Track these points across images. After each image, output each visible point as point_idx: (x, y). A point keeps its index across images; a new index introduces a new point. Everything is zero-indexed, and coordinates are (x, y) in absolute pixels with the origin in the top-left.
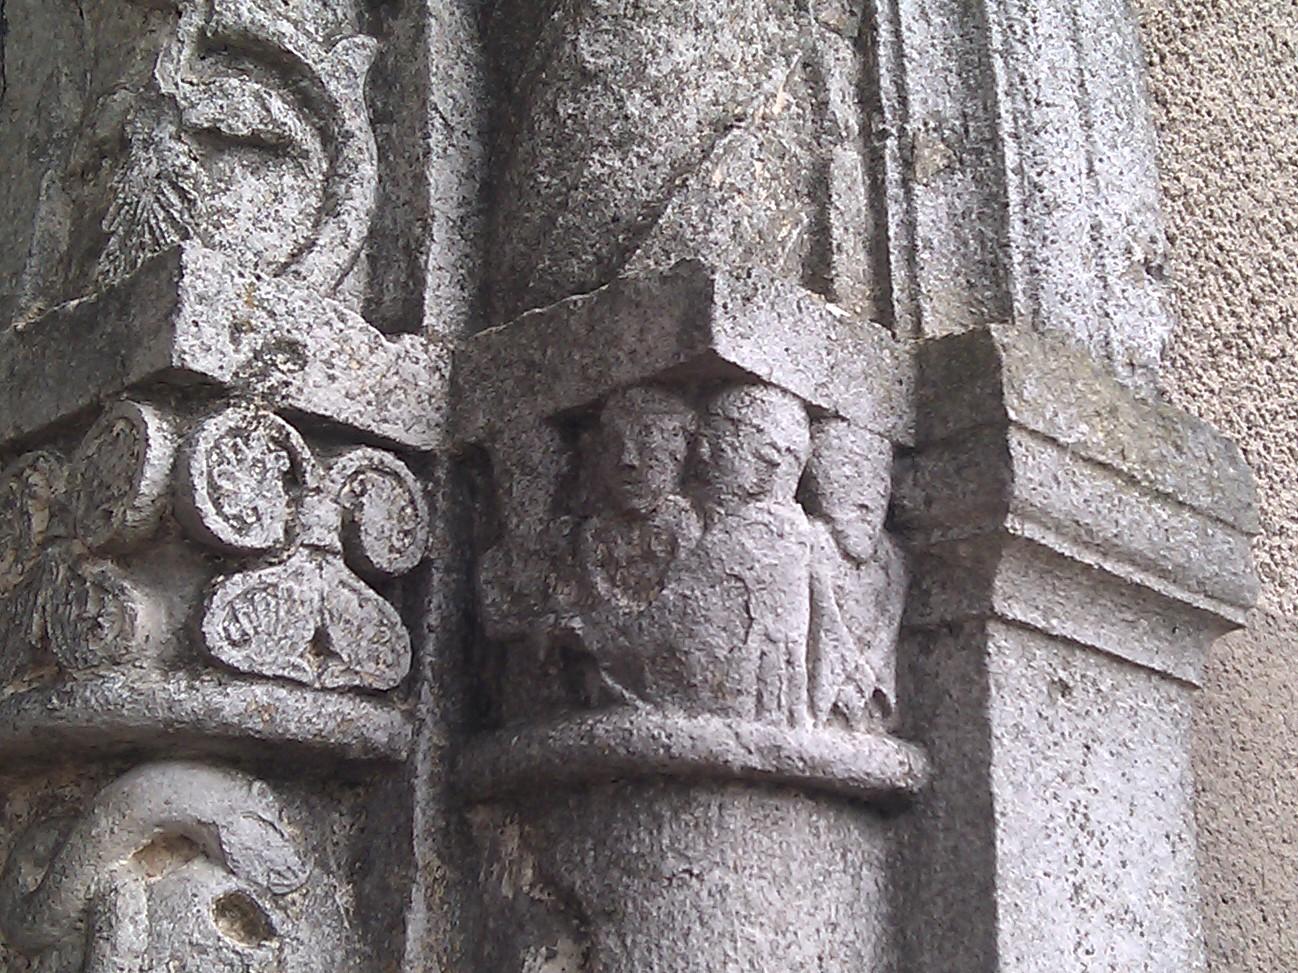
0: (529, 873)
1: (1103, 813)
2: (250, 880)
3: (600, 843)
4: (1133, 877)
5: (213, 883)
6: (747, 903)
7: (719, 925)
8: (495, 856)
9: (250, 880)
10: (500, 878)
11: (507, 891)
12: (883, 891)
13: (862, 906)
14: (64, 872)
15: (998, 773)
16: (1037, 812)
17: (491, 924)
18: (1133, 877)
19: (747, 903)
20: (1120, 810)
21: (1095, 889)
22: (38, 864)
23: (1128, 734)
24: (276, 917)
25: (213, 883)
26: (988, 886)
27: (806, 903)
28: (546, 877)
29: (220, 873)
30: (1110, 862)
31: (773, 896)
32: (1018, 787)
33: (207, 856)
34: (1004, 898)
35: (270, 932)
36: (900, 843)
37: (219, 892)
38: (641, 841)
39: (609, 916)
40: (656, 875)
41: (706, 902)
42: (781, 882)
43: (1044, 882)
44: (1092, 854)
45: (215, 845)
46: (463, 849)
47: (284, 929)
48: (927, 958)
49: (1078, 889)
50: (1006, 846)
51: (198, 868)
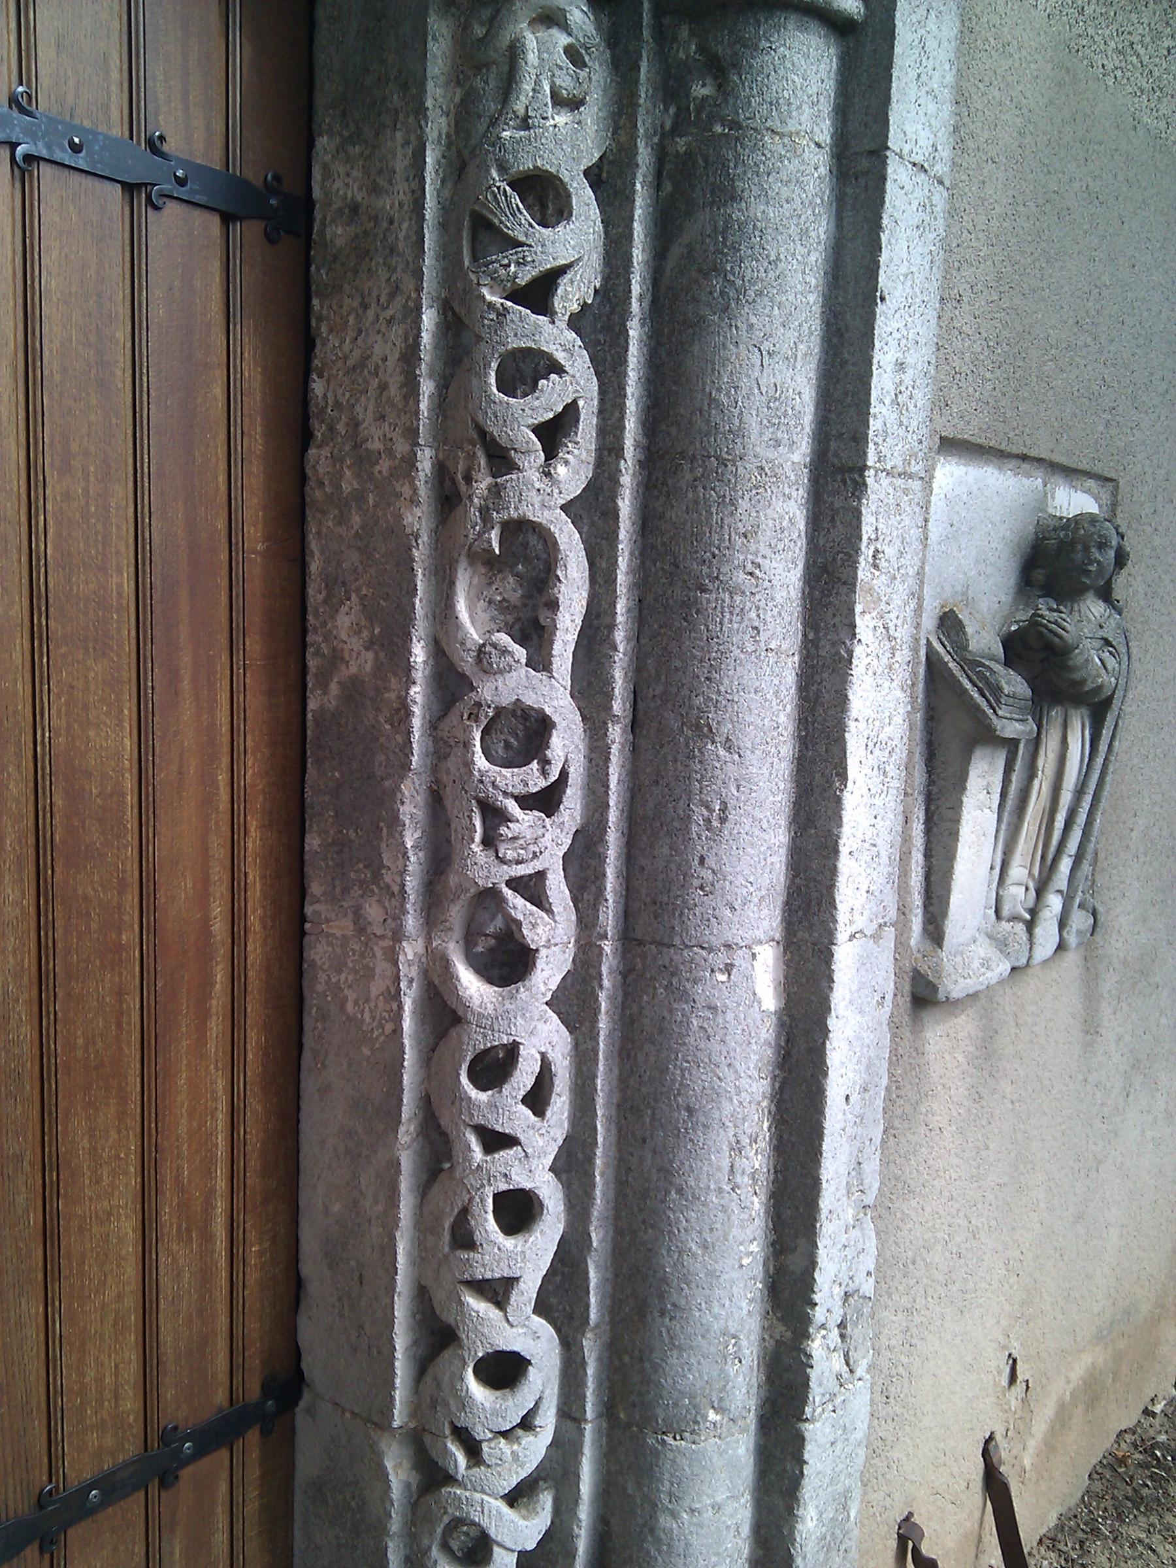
0: (694, 47)
1: (931, 44)
2: (577, 40)
3: (731, 32)
4: (937, 75)
5: (563, 40)
6: (793, 64)
7: (782, 72)
8: (675, 39)
9: (577, 40)
10: (678, 51)
11: (682, 55)
12: (839, 68)
13: (832, 75)
14: (500, 27)
15: (898, 14)
16: (910, 37)
17: (673, 71)
18: (937, 75)
19: (793, 64)
20: (935, 44)
21: (924, 78)
22: (482, 24)
23: (942, 8)
24: (587, 58)
25: (563, 40)
26: (889, 67)
27: (814, 68)
28: (701, 49)
29: (565, 35)
30: (930, 67)
31: (803, 63)
32: (904, 23)
33: (558, 25)
34: (895, 73)
35: (585, 65)
36: (848, 48)
37: (566, 43)
38: (750, 32)
39: (734, 66)
40: (756, 48)
41: (777, 62)
42: (807, 56)
43: (909, 70)
44: (924, 63)
45: (563, 20)
46: (662, 36)
47: (590, 64)
48: (857, 100)
49: (919, 76)
50: (898, 50)
51: (555, 32)
